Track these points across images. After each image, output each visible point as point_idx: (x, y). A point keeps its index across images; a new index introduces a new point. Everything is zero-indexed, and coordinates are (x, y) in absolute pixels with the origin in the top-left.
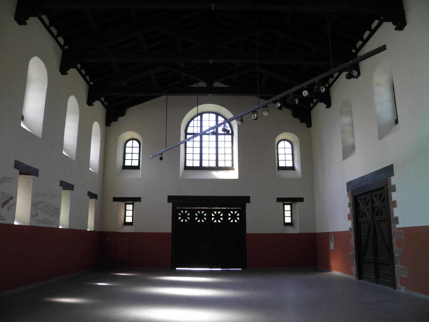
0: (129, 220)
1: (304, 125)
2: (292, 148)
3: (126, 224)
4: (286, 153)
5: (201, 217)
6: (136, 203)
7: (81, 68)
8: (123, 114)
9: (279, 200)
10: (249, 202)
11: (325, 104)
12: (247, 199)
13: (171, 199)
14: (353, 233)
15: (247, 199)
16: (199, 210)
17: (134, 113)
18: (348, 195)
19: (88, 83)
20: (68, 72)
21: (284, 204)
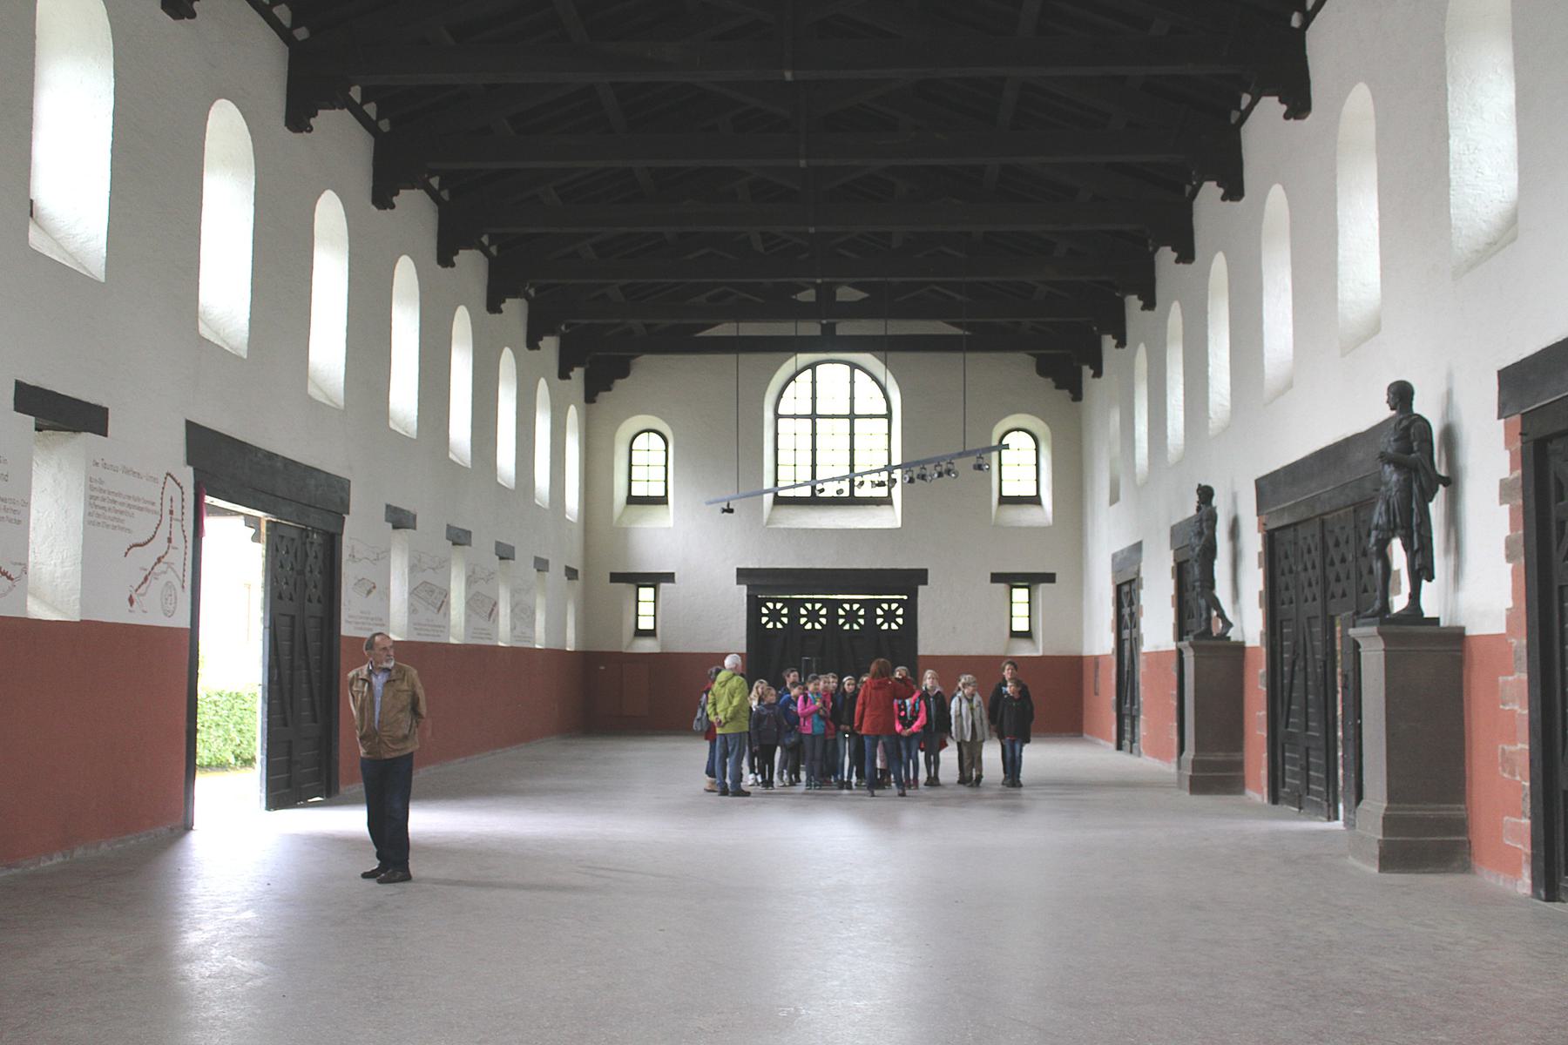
0: (646, 623)
1: (1065, 394)
2: (1037, 450)
3: (641, 633)
4: (1021, 464)
5: (813, 616)
6: (663, 586)
7: (365, 100)
8: (624, 373)
9: (996, 578)
10: (925, 583)
11: (1219, 185)
12: (920, 576)
13: (743, 575)
14: (1520, 642)
15: (920, 576)
16: (809, 601)
17: (650, 370)
18: (1508, 444)
19: (285, 34)
20: (395, 199)
21: (1012, 587)
